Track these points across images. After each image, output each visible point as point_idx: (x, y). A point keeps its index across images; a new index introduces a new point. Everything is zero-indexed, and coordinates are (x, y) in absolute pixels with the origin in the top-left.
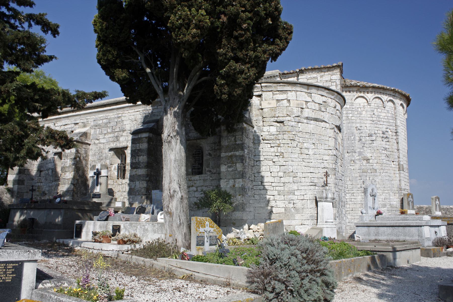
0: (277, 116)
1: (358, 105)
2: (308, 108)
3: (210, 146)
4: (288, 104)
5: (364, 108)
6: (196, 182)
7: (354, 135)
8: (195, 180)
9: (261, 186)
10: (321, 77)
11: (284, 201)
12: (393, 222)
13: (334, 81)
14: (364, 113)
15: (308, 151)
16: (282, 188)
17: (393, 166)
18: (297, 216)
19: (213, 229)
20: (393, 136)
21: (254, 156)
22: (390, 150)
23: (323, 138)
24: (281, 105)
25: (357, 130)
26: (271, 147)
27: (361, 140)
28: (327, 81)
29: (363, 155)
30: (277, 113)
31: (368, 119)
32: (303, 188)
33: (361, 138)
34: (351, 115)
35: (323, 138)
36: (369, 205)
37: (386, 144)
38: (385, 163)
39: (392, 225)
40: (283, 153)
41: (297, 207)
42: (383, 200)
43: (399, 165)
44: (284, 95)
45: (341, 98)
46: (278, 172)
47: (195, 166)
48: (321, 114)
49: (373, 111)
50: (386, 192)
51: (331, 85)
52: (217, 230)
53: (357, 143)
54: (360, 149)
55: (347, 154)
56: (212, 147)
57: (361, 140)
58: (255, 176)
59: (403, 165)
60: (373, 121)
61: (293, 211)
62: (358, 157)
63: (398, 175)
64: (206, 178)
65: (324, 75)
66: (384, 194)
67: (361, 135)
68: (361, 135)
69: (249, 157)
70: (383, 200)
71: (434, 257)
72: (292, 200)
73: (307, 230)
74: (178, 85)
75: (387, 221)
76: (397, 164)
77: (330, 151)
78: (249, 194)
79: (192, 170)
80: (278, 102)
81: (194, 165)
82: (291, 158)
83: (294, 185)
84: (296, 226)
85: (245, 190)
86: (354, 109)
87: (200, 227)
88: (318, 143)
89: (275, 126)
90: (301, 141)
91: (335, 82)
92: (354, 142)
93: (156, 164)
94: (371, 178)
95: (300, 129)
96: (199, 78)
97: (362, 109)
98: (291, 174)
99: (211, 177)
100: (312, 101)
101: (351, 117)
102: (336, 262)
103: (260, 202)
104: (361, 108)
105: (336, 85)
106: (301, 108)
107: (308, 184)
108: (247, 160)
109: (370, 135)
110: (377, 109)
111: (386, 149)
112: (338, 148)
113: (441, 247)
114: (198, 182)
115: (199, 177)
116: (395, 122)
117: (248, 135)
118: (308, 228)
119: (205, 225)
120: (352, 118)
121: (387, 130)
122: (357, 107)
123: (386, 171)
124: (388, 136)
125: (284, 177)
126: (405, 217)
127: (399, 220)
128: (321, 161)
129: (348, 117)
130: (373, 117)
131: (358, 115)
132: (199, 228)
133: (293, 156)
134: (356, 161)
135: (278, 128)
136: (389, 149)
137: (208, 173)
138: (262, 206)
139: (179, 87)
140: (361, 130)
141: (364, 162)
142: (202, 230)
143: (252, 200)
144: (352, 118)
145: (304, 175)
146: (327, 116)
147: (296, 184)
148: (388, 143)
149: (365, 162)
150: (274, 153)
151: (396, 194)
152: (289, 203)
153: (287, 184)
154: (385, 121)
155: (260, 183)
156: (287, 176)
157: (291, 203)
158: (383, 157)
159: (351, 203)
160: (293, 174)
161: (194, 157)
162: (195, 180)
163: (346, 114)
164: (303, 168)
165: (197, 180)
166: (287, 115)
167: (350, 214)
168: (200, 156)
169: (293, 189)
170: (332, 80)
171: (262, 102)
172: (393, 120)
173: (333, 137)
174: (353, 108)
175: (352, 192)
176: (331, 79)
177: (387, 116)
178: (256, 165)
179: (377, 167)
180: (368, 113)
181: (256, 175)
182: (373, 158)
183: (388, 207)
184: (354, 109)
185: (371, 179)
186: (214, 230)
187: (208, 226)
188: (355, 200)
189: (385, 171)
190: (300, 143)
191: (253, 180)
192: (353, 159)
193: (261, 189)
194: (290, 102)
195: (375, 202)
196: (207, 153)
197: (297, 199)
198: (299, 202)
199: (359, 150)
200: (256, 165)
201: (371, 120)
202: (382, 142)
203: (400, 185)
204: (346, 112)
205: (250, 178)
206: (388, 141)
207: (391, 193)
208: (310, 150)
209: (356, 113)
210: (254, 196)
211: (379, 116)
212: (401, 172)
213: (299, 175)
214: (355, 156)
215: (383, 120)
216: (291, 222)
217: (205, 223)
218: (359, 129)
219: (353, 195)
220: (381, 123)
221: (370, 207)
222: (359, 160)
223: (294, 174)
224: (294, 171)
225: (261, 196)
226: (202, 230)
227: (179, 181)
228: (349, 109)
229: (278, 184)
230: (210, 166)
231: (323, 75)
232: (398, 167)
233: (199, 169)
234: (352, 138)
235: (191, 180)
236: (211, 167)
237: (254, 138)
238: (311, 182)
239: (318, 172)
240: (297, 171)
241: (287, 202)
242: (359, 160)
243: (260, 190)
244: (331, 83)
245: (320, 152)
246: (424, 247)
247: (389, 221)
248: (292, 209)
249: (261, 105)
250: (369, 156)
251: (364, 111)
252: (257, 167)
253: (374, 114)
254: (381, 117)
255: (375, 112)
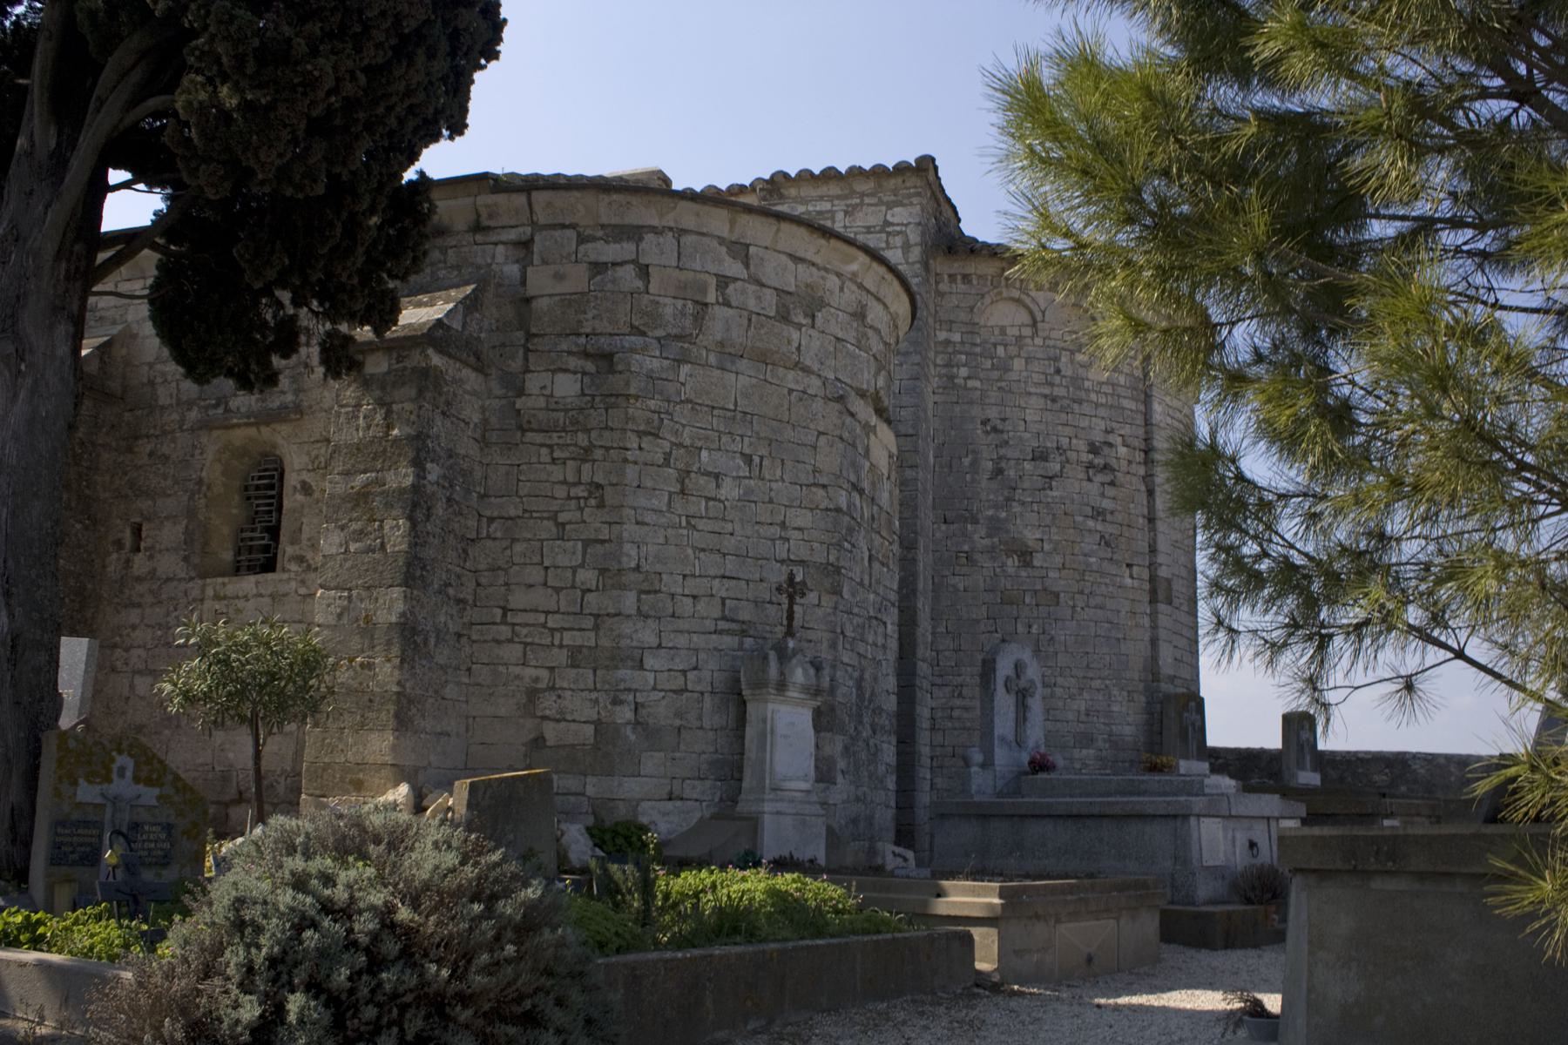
0: (588, 330)
1: (997, 332)
2: (727, 304)
3: (308, 454)
4: (640, 284)
5: (1021, 348)
6: (240, 604)
7: (974, 452)
8: (238, 597)
9: (503, 628)
10: (846, 213)
11: (594, 695)
12: (1083, 800)
13: (898, 228)
14: (1018, 364)
15: (718, 486)
16: (589, 639)
17: (1128, 581)
18: (652, 762)
19: (156, 791)
20: (1134, 465)
21: (482, 497)
22: (1119, 517)
23: (789, 433)
24: (609, 286)
25: (987, 433)
26: (553, 459)
27: (999, 471)
28: (868, 228)
29: (1007, 532)
30: (590, 315)
31: (1033, 390)
32: (682, 641)
33: (1003, 464)
34: (964, 372)
35: (789, 433)
36: (998, 731)
37: (1103, 495)
38: (1095, 568)
39: (1075, 812)
40: (599, 486)
41: (651, 721)
42: (1083, 718)
43: (1153, 579)
44: (625, 245)
45: (889, 277)
46: (574, 570)
47: (252, 539)
48: (785, 334)
49: (1056, 359)
50: (1097, 683)
51: (883, 245)
52: (176, 798)
53: (984, 483)
54: (996, 507)
55: (944, 527)
56: (317, 457)
57: (999, 471)
58: (478, 584)
59: (1169, 581)
60: (1054, 400)
61: (633, 737)
62: (987, 542)
63: (1146, 621)
64: (283, 589)
65: (862, 204)
66: (1086, 695)
67: (1002, 451)
68: (1002, 451)
69: (449, 500)
70: (1083, 718)
71: (1226, 947)
72: (629, 690)
73: (695, 821)
74: (53, 131)
75: (1064, 796)
76: (1146, 576)
77: (821, 492)
78: (441, 660)
79: (238, 552)
80: (599, 273)
81: (245, 535)
82: (635, 509)
83: (640, 625)
84: (645, 805)
85: (419, 639)
86: (978, 350)
87: (81, 781)
88: (764, 451)
89: (575, 373)
90: (688, 442)
91: (899, 233)
92: (973, 481)
93: (86, 528)
94: (1035, 627)
95: (687, 392)
96: (133, 103)
97: (1013, 350)
98: (633, 577)
99: (303, 582)
100: (750, 276)
101: (965, 379)
102: (667, 961)
103: (491, 695)
104: (1005, 346)
105: (906, 247)
106: (696, 302)
107: (710, 625)
108: (440, 510)
109: (1040, 456)
110: (1072, 352)
111: (1099, 514)
112: (866, 485)
113: (1261, 908)
114: (251, 604)
115: (257, 583)
116: (1142, 408)
117: (448, 404)
118: (699, 815)
119: (109, 771)
120: (970, 383)
121: (1111, 438)
122: (993, 340)
123: (1099, 600)
124: (1113, 463)
125: (597, 589)
126: (1133, 781)
127: (1109, 794)
128: (776, 531)
129: (952, 378)
130: (1052, 385)
131: (995, 375)
132: (75, 783)
133: (643, 502)
134: (977, 556)
135: (587, 380)
136: (1112, 513)
137: (294, 567)
138: (502, 712)
139: (59, 144)
140: (1002, 432)
141: (1010, 562)
142: (87, 792)
143: (458, 684)
144: (970, 383)
145: (692, 586)
146: (816, 344)
147: (649, 621)
148: (1110, 491)
149: (1012, 563)
150: (565, 487)
151: (1136, 696)
152: (616, 702)
153: (610, 621)
154: (1104, 401)
155: (499, 612)
156: (613, 587)
157: (621, 702)
158: (1089, 544)
159: (950, 725)
160: (641, 577)
161: (249, 498)
162: (238, 597)
163: (945, 366)
164: (687, 557)
165: (246, 598)
166: (632, 326)
167: (945, 771)
168: (272, 497)
169: (635, 644)
170: (893, 224)
171: (529, 270)
172: (1137, 401)
173: (837, 432)
174: (975, 345)
175: (959, 680)
176: (887, 223)
177: (1113, 385)
178: (488, 537)
179: (1062, 582)
180: (1035, 366)
181: (483, 581)
182: (1047, 547)
183: (1100, 744)
184: (978, 350)
185: (1034, 630)
186: (159, 798)
187: (129, 774)
188: (965, 715)
189: (1093, 602)
190: (682, 451)
191: (470, 598)
192: (966, 548)
193: (503, 638)
194: (648, 274)
195: (1025, 719)
196: (293, 483)
197: (654, 689)
198: (664, 703)
199: (990, 513)
200: (488, 537)
201: (1045, 396)
202: (1085, 483)
203: (1154, 658)
204: (946, 357)
205: (451, 591)
206: (1112, 484)
207: (1115, 692)
208: (727, 483)
209: (988, 364)
210: (469, 669)
211: (1077, 381)
212: (1162, 607)
213: (671, 583)
214: (976, 537)
215: (1093, 397)
216: (620, 785)
217: (113, 760)
218: (995, 430)
219: (960, 695)
220: (1086, 409)
221: (1003, 739)
222: (991, 551)
223: (646, 580)
224: (645, 567)
225: (501, 668)
226: (87, 792)
227: (10, 563)
228: (958, 347)
229: (571, 618)
230: (304, 536)
231: (857, 205)
232: (1147, 586)
233: (266, 549)
234: (966, 461)
235: (225, 598)
236: (304, 542)
237: (485, 421)
238: (724, 618)
239: (757, 576)
240: (658, 568)
241: (604, 698)
242: (991, 551)
243: (498, 642)
244: (884, 236)
245: (773, 494)
246: (1193, 904)
247: (1071, 796)
248: (629, 731)
249: (523, 282)
250: (1031, 536)
251: (1019, 356)
252: (489, 543)
253: (1058, 371)
254: (1087, 384)
255: (1062, 365)
